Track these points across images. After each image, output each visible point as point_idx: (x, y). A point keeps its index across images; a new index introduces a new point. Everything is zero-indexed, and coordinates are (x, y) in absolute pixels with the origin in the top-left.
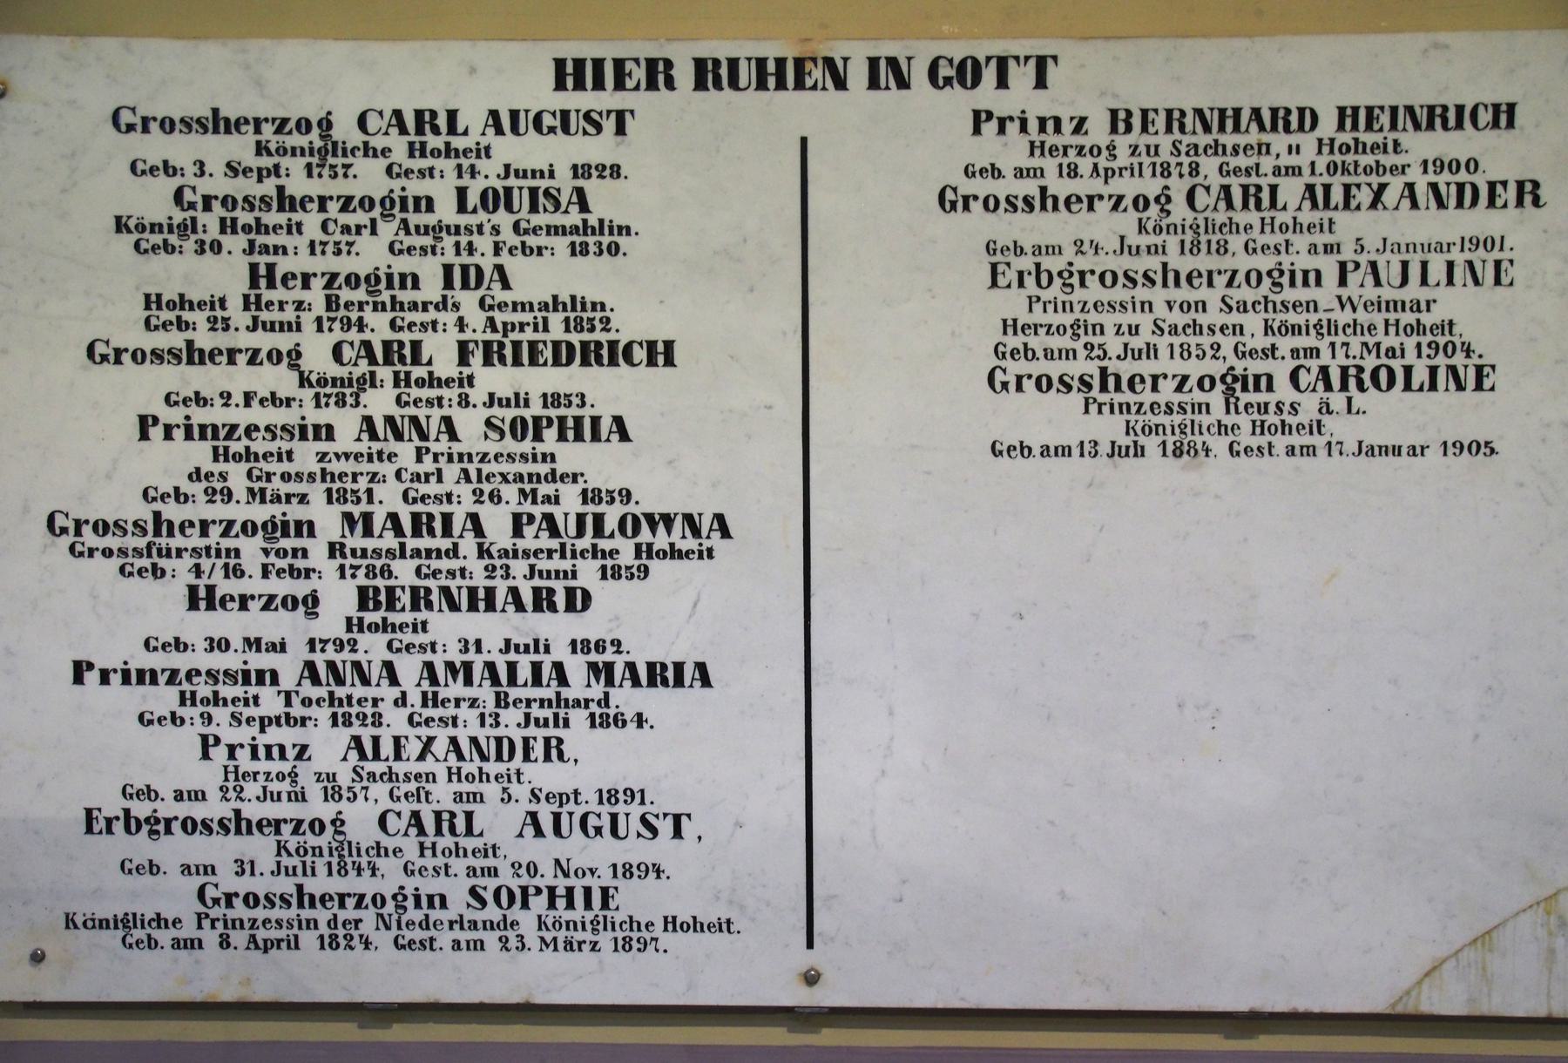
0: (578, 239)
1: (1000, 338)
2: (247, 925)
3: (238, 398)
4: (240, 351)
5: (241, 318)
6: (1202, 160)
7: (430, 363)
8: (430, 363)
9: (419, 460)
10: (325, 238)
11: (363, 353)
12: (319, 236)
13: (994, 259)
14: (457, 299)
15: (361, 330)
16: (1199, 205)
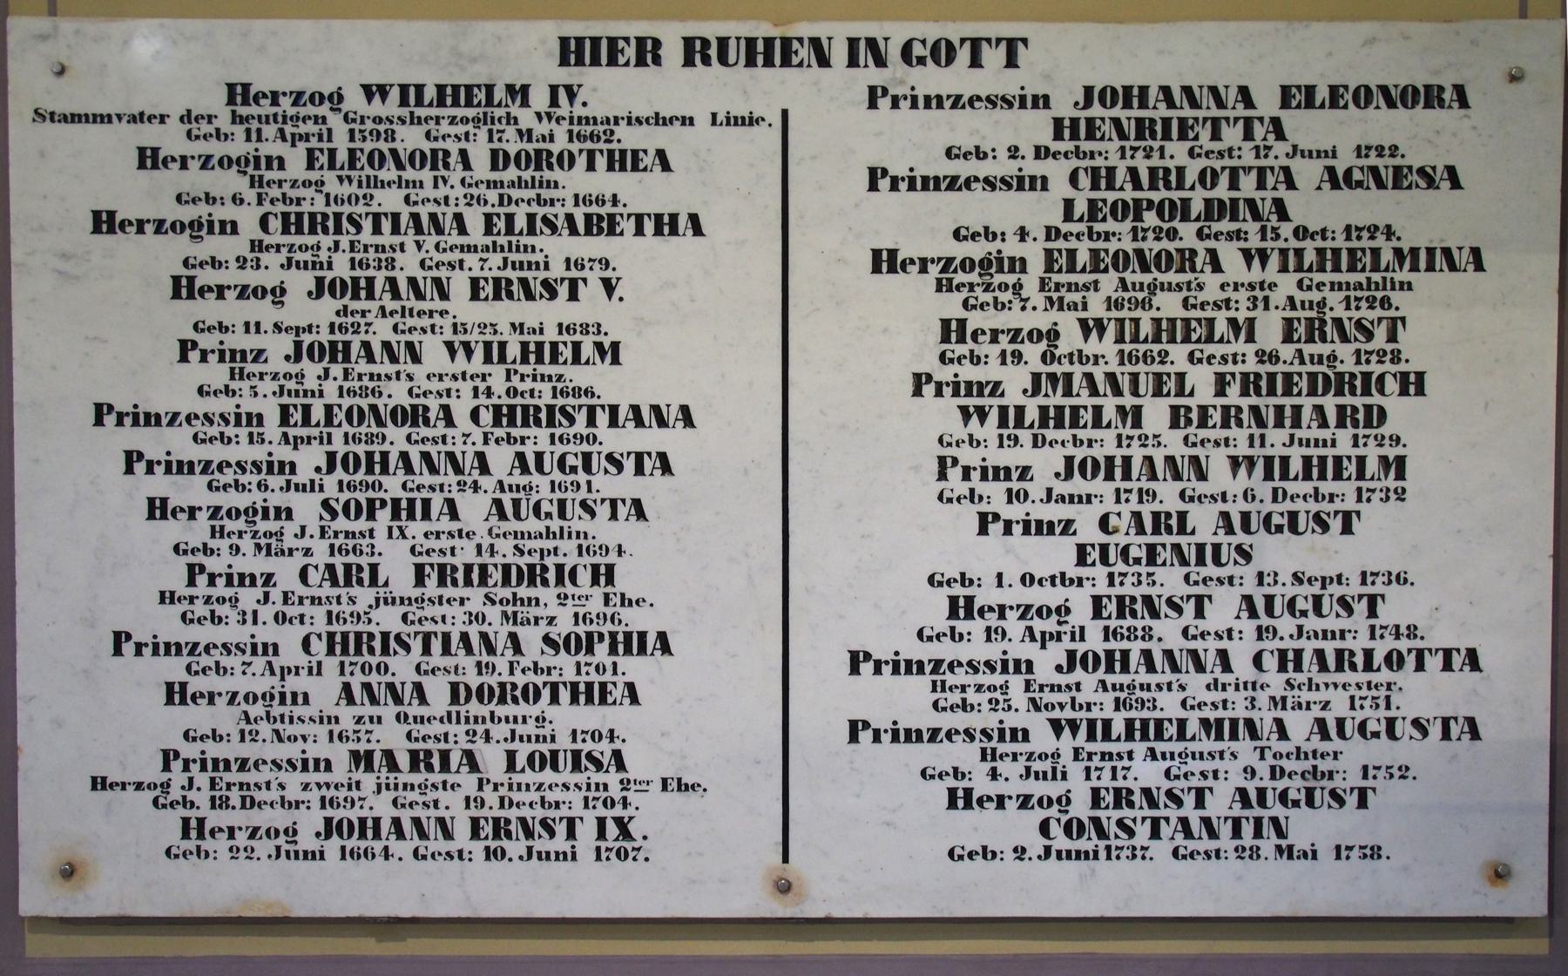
0: (510, 609)
1: (135, 639)
2: (260, 582)
3: (1227, 755)
4: (229, 287)
5: (1038, 299)
6: (265, 127)
7: (386, 584)
8: (386, 584)
9: (192, 582)
10: (1104, 539)
11: (1466, 729)
12: (1096, 537)
13: (420, 560)
14: (1182, 681)
15: (612, 740)
16: (313, 650)
